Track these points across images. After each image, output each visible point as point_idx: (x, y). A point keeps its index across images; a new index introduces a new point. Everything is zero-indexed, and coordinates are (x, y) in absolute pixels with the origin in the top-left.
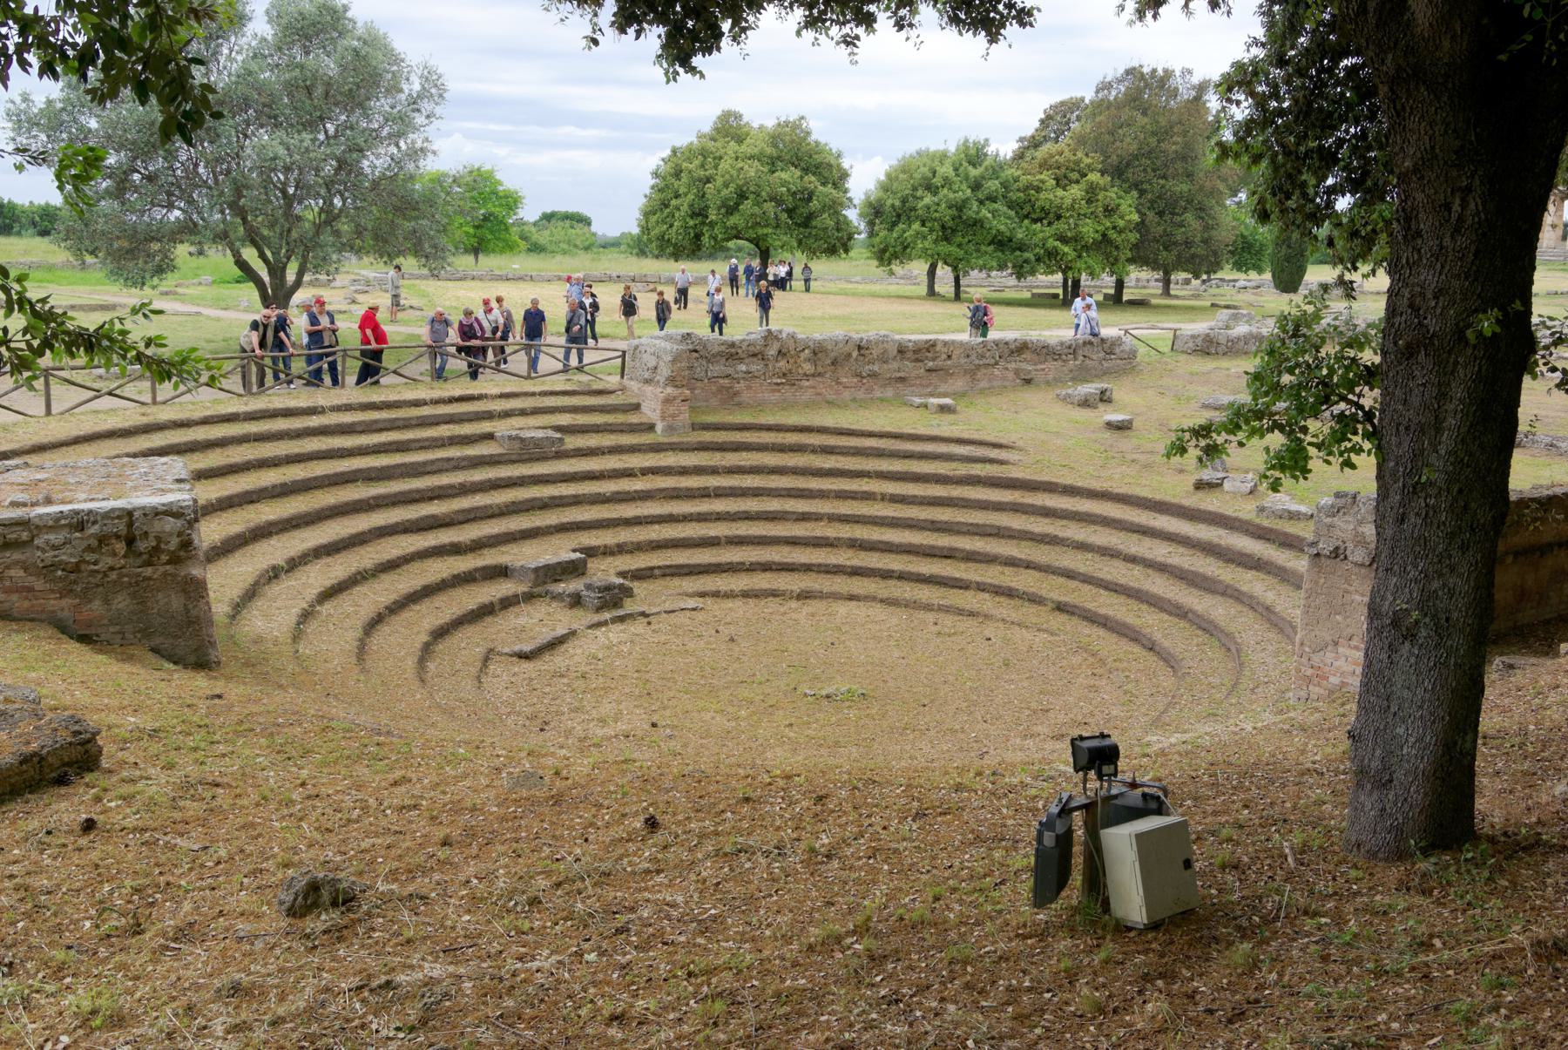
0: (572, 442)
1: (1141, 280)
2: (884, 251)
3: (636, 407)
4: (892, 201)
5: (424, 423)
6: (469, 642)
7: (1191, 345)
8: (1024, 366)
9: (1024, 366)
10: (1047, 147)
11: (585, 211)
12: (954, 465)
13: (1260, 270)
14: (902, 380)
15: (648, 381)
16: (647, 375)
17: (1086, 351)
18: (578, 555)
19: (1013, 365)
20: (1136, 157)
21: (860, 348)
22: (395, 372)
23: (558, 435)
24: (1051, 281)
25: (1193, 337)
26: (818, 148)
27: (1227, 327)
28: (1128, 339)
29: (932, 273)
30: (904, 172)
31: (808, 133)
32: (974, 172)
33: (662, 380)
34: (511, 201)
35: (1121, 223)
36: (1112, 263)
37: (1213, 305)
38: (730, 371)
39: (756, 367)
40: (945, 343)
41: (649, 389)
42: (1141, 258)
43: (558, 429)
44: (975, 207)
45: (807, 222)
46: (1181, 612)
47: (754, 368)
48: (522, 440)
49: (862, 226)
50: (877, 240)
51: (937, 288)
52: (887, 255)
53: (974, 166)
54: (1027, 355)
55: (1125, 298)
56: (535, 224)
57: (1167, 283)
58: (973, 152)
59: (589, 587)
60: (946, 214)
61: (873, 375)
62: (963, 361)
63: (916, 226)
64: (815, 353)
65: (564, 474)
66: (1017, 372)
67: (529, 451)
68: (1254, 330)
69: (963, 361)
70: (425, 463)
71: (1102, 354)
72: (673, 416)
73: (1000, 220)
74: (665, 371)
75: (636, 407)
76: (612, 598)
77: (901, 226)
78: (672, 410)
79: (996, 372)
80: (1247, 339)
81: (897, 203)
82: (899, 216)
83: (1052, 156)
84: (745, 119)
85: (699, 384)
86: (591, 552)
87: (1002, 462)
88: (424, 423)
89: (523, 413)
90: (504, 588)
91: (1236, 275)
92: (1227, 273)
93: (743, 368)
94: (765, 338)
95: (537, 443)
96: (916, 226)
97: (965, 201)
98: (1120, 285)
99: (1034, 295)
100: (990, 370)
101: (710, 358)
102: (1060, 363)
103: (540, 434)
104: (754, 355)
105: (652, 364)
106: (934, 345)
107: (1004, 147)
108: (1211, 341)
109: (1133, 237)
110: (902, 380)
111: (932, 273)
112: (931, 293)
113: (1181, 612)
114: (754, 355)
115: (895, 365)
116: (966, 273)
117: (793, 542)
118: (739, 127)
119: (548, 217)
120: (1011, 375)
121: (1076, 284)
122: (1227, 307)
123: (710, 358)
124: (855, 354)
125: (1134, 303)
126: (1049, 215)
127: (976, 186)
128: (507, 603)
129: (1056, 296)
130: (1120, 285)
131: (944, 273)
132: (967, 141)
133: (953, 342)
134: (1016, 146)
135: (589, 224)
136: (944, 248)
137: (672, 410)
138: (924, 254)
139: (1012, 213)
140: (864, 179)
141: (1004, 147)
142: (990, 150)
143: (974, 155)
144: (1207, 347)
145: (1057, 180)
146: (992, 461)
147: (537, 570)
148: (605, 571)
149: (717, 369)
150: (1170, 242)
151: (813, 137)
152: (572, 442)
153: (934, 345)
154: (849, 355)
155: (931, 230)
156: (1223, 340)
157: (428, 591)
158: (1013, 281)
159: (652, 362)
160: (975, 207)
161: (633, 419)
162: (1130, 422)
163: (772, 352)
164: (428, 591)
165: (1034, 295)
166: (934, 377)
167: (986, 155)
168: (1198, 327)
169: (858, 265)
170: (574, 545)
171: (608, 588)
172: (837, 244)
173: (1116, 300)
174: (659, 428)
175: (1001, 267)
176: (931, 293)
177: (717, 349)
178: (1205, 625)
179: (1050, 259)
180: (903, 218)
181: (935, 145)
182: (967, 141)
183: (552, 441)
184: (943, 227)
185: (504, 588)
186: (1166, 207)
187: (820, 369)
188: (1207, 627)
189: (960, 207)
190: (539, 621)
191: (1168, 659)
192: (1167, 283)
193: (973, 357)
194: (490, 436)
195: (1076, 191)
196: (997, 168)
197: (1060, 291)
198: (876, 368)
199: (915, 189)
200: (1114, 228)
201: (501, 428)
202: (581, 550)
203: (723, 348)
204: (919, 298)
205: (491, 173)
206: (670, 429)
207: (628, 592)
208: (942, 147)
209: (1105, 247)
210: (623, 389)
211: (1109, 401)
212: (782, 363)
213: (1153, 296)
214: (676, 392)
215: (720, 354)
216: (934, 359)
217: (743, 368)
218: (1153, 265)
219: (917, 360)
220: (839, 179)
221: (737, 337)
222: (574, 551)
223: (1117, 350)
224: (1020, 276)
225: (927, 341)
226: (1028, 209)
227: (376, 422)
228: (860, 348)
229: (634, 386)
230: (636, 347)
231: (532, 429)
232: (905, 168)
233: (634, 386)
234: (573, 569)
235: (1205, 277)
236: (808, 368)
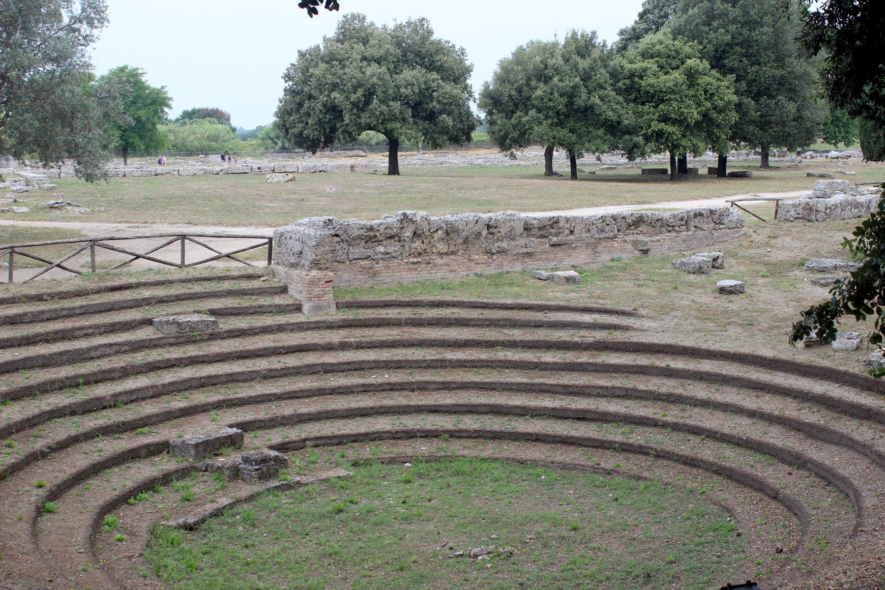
0: (227, 324)
1: (740, 157)
2: (505, 137)
3: (284, 290)
4: (508, 91)
5: (86, 311)
6: (138, 517)
7: (793, 213)
8: (640, 237)
9: (640, 237)
10: (648, 39)
11: (223, 107)
12: (583, 332)
13: (848, 144)
14: (529, 255)
15: (293, 266)
16: (293, 260)
17: (696, 222)
18: (235, 430)
19: (631, 238)
20: (730, 46)
21: (489, 227)
22: (58, 266)
23: (213, 319)
24: (661, 159)
25: (793, 205)
26: (440, 48)
27: (825, 196)
28: (734, 210)
29: (549, 155)
30: (518, 63)
31: (430, 32)
32: (583, 64)
33: (307, 263)
34: (157, 101)
35: (721, 103)
36: (715, 143)
37: (809, 175)
38: (369, 252)
39: (393, 247)
40: (568, 220)
41: (295, 272)
42: (738, 135)
43: (213, 312)
44: (584, 96)
45: (431, 117)
46: (798, 462)
47: (391, 249)
48: (179, 324)
49: (482, 115)
50: (496, 128)
51: (555, 169)
52: (508, 141)
53: (583, 56)
54: (643, 228)
55: (728, 171)
56: (177, 120)
57: (765, 156)
58: (582, 43)
59: (246, 460)
60: (561, 103)
61: (502, 252)
62: (584, 235)
63: (532, 112)
64: (447, 234)
65: (219, 355)
66: (635, 243)
67: (186, 335)
68: (850, 198)
69: (584, 235)
70: (89, 350)
71: (712, 225)
72: (319, 297)
73: (612, 106)
74: (309, 256)
75: (284, 290)
76: (267, 468)
77: (519, 113)
78: (317, 291)
79: (616, 245)
80: (843, 206)
81: (513, 93)
82: (516, 105)
83: (654, 45)
84: (368, 20)
85: (341, 266)
86: (245, 427)
87: (627, 328)
88: (86, 311)
89: (179, 298)
90: (164, 464)
91: (827, 146)
92: (819, 144)
93: (382, 249)
94: (401, 221)
95: (193, 326)
96: (532, 112)
97: (575, 87)
98: (723, 161)
99: (643, 171)
100: (610, 243)
101: (351, 242)
102: (673, 234)
103: (195, 318)
104: (391, 237)
105: (296, 250)
106: (557, 222)
107: (608, 37)
108: (811, 209)
109: (734, 117)
110: (529, 255)
111: (549, 155)
112: (550, 172)
113: (798, 462)
114: (391, 237)
115: (522, 241)
116: (581, 155)
117: (435, 410)
118: (363, 29)
119: (190, 115)
120: (629, 247)
121: (683, 161)
122: (822, 176)
123: (351, 242)
124: (485, 232)
125: (734, 175)
126: (655, 97)
127: (586, 77)
128: (166, 479)
129: (664, 171)
130: (723, 161)
131: (560, 157)
132: (574, 34)
133: (575, 218)
134: (618, 38)
135: (228, 120)
136: (562, 133)
137: (317, 291)
138: (540, 141)
139: (620, 98)
140: (481, 77)
141: (608, 37)
142: (599, 41)
143: (582, 46)
144: (808, 214)
145: (661, 67)
146: (616, 327)
147: (197, 446)
148: (259, 444)
149: (358, 251)
150: (766, 127)
151: (434, 37)
152: (227, 324)
153: (557, 222)
154: (480, 234)
155: (547, 117)
156: (821, 208)
157: (97, 469)
158: (624, 160)
159: (297, 248)
160: (584, 96)
161: (278, 300)
162: (742, 286)
163: (408, 233)
164: (97, 469)
165: (643, 171)
166: (559, 253)
167: (594, 46)
168: (797, 195)
169: (483, 157)
170: (233, 420)
171: (265, 460)
172: (460, 136)
173: (720, 171)
174: (306, 307)
175: (614, 147)
176: (550, 172)
177: (356, 233)
178: (823, 473)
179: (659, 139)
180: (521, 107)
181: (547, 38)
182: (574, 34)
183: (207, 324)
184: (558, 113)
185: (164, 464)
186: (758, 91)
187: (452, 248)
188: (827, 477)
189: (570, 95)
190: (208, 493)
191: (791, 507)
192: (765, 156)
193: (594, 232)
194: (149, 322)
195: (677, 76)
196: (606, 58)
197: (669, 168)
198: (504, 245)
199: (529, 79)
200: (714, 108)
201: (159, 314)
202: (238, 425)
203: (362, 232)
204: (538, 177)
205: (123, 69)
206: (318, 308)
207: (282, 463)
208: (552, 39)
209: (707, 129)
210: (274, 274)
211: (721, 267)
212: (417, 244)
213: (755, 168)
214: (320, 274)
215: (360, 237)
216: (557, 235)
217: (382, 249)
218: (751, 142)
219: (542, 236)
220: (457, 74)
221: (105, 73)
222: (231, 426)
223: (726, 221)
224: (631, 158)
225: (550, 219)
226: (633, 90)
227: (42, 312)
228: (489, 227)
229: (281, 269)
230: (282, 235)
231: (190, 315)
232: (520, 56)
233: (281, 269)
234: (233, 442)
235: (799, 149)
236: (442, 247)
